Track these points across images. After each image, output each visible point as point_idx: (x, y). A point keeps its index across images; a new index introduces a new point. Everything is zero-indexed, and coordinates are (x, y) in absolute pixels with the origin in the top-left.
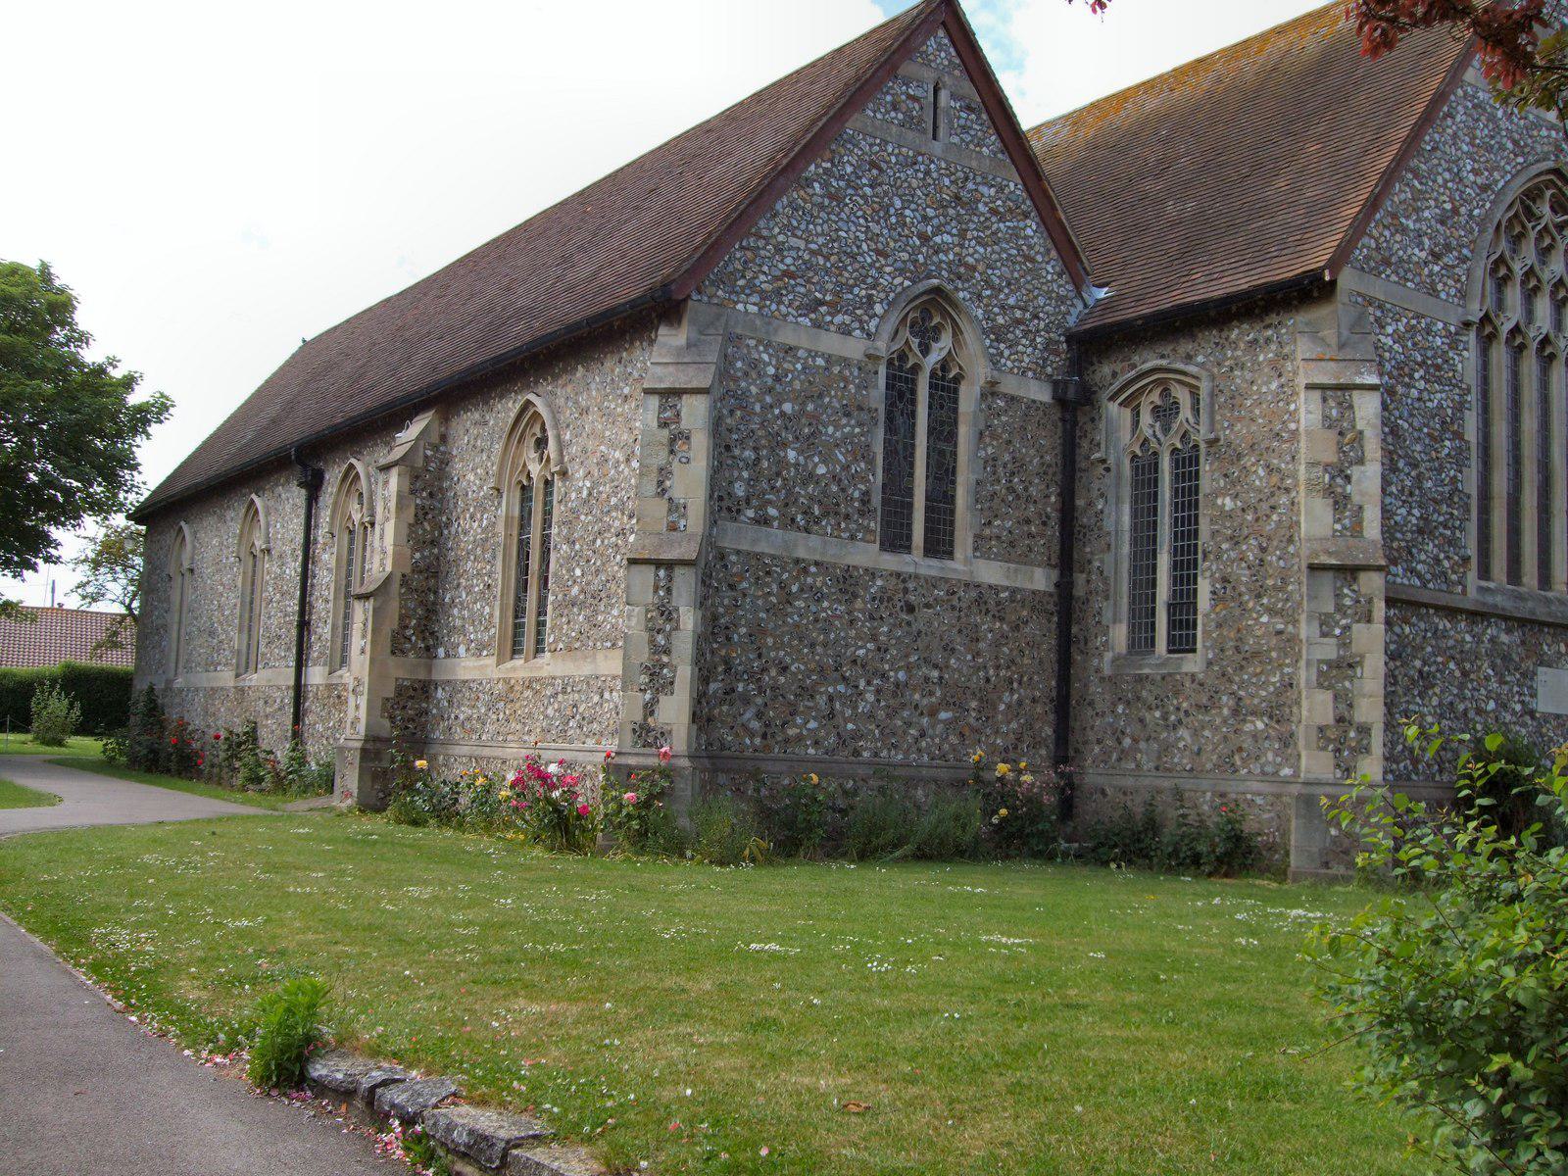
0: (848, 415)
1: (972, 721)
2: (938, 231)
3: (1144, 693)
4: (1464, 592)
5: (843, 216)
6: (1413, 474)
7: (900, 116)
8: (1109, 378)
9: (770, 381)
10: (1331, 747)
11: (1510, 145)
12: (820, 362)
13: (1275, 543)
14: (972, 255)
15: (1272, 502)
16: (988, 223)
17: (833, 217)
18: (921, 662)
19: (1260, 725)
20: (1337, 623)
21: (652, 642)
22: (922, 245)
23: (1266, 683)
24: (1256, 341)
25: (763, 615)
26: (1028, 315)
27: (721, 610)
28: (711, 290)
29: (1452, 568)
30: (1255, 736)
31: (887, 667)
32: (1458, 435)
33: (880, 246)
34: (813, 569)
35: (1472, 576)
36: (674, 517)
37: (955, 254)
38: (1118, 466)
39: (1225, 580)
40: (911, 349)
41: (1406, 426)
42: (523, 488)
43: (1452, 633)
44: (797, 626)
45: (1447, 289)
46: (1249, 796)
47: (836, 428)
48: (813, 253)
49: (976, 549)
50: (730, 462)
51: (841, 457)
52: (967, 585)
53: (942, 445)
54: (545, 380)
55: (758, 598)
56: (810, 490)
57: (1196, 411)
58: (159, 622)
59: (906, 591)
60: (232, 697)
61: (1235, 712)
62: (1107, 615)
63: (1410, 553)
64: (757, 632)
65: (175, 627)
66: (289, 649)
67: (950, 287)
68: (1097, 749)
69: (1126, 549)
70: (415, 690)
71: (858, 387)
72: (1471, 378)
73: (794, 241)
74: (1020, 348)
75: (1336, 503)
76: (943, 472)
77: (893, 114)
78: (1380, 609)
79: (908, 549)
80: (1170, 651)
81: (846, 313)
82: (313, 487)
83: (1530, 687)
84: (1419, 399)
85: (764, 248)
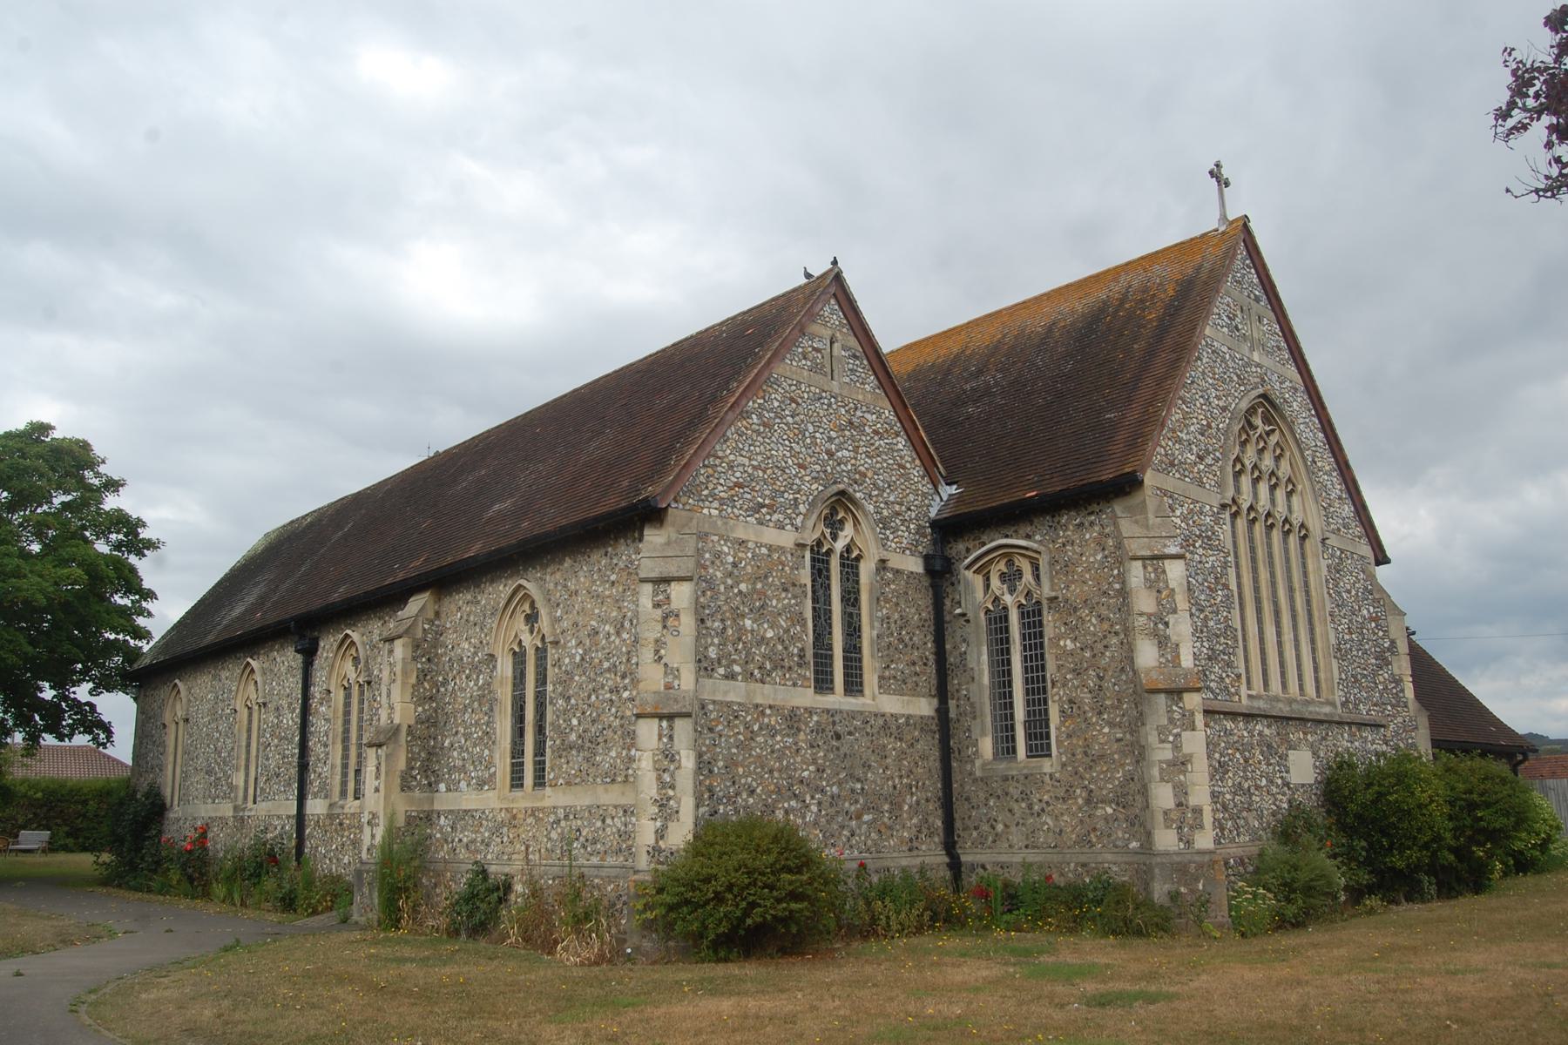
0: (786, 590)
1: (886, 820)
3: (1011, 790)
5: (773, 439)
6: (1202, 616)
7: (809, 363)
8: (964, 552)
9: (730, 567)
10: (1174, 826)
11: (1235, 378)
12: (764, 550)
14: (863, 465)
15: (1105, 642)
16: (872, 441)
17: (767, 440)
19: (1110, 811)
20: (1170, 732)
21: (659, 778)
22: (829, 459)
23: (1112, 778)
24: (1081, 524)
25: (734, 750)
26: (903, 508)
27: (704, 749)
28: (684, 499)
29: (1231, 684)
30: (1106, 818)
31: (824, 783)
32: (1226, 586)
33: (801, 461)
34: (768, 711)
35: (1244, 688)
37: (852, 465)
39: (1071, 702)
40: (825, 537)
41: (1194, 582)
42: (515, 653)
44: (759, 756)
45: (1209, 481)
46: (1106, 865)
48: (754, 468)
49: (880, 687)
51: (783, 623)
52: (876, 715)
53: (850, 609)
54: (534, 568)
55: (730, 737)
56: (763, 650)
57: (1037, 577)
58: (155, 762)
59: (834, 723)
60: (230, 824)
61: (1088, 801)
63: (1205, 675)
64: (731, 764)
65: (170, 767)
66: (289, 785)
67: (851, 490)
69: (986, 680)
70: (421, 819)
71: (792, 569)
72: (1229, 545)
75: (1160, 642)
76: (853, 630)
77: (804, 362)
78: (1199, 719)
79: (831, 690)
81: (780, 513)
84: (1200, 562)
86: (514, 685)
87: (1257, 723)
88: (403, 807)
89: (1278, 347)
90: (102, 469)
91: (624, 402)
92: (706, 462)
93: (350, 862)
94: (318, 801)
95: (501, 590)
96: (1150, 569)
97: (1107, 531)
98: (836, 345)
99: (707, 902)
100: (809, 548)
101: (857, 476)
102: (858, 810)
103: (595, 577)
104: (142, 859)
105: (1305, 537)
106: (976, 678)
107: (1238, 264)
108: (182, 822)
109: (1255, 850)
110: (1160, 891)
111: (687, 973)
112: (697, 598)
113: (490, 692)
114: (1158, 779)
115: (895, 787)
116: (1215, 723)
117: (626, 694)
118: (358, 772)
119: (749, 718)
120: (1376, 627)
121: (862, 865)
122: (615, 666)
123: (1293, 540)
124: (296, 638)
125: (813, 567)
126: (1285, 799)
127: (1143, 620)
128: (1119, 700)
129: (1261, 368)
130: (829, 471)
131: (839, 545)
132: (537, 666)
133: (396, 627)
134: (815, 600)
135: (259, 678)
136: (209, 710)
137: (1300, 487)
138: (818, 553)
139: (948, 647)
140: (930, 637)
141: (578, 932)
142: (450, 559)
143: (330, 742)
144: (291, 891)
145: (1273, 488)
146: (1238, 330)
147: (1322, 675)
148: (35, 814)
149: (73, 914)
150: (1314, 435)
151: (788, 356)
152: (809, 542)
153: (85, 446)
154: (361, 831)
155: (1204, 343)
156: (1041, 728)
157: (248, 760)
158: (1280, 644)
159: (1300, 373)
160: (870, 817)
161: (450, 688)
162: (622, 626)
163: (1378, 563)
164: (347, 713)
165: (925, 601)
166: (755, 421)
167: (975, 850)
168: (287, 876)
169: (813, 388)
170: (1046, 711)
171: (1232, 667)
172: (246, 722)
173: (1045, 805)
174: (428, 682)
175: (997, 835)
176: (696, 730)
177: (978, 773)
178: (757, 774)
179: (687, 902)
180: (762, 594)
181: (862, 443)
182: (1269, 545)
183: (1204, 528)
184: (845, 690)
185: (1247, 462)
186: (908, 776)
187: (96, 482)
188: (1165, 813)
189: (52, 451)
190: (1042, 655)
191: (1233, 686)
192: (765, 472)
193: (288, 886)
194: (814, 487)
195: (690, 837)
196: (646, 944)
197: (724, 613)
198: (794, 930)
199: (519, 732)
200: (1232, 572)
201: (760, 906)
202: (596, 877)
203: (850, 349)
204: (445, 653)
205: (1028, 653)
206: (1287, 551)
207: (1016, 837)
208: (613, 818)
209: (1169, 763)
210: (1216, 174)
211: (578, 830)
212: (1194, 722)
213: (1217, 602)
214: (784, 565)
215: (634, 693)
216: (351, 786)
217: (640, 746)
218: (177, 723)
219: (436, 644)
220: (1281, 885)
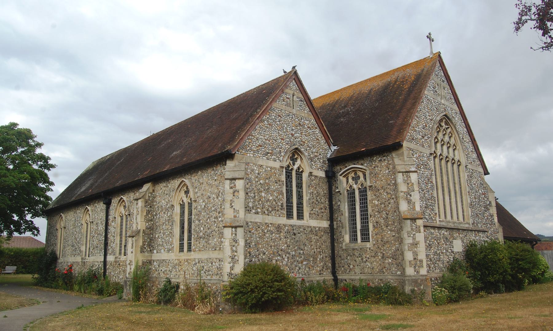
0: (276, 183)
1: (311, 264)
2: (296, 133)
4: (436, 222)
5: (272, 129)
6: (423, 193)
7: (285, 103)
8: (339, 170)
10: (413, 266)
11: (435, 109)
12: (269, 169)
15: (389, 202)
16: (307, 131)
17: (270, 130)
18: (298, 249)
19: (390, 261)
20: (412, 233)
21: (232, 249)
24: (381, 160)
25: (258, 239)
26: (318, 154)
27: (247, 238)
28: (241, 151)
31: (290, 251)
32: (432, 182)
33: (282, 137)
34: (270, 225)
36: (236, 213)
38: (343, 193)
39: (377, 222)
40: (290, 164)
42: (181, 205)
43: (435, 233)
44: (267, 241)
45: (426, 145)
46: (389, 280)
48: (266, 140)
49: (310, 217)
50: (248, 197)
51: (275, 194)
52: (308, 227)
53: (299, 190)
55: (257, 234)
56: (268, 204)
57: (365, 179)
59: (293, 230)
60: (80, 264)
61: (383, 257)
62: (343, 233)
63: (424, 213)
64: (257, 244)
65: (59, 244)
67: (300, 148)
68: (343, 269)
69: (347, 215)
70: (147, 263)
71: (279, 175)
72: (433, 168)
73: (261, 137)
74: (317, 163)
75: (408, 202)
76: (300, 197)
77: (283, 102)
78: (422, 229)
80: (362, 242)
81: (275, 155)
82: (108, 204)
83: (452, 245)
84: (423, 174)
85: (254, 139)
87: (442, 230)
88: (141, 258)
89: (450, 98)
90: (35, 139)
92: (249, 138)
93: (122, 278)
94: (111, 256)
95: (175, 183)
96: (405, 176)
97: (390, 162)
98: (295, 97)
99: (248, 292)
100: (285, 168)
101: (302, 143)
102: (301, 260)
103: (209, 178)
104: (49, 276)
106: (343, 214)
107: (437, 69)
108: (63, 263)
109: (441, 275)
110: (408, 289)
112: (245, 185)
113: (172, 218)
115: (315, 252)
116: (428, 230)
117: (220, 219)
118: (125, 246)
119: (263, 228)
120: (484, 197)
122: (216, 209)
123: (455, 166)
125: (286, 175)
126: (452, 257)
127: (402, 194)
129: (444, 105)
130: (292, 141)
131: (295, 167)
132: (189, 209)
134: (287, 186)
135: (90, 213)
137: (458, 148)
138: (288, 170)
139: (333, 203)
140: (327, 200)
141: (203, 302)
142: (158, 171)
143: (115, 235)
144: (102, 288)
146: (436, 92)
147: (465, 214)
149: (25, 296)
151: (278, 100)
152: (285, 166)
153: (29, 131)
154: (127, 267)
155: (424, 97)
157: (86, 242)
160: (306, 263)
162: (219, 195)
163: (485, 174)
164: (121, 225)
165: (325, 187)
166: (266, 123)
167: (343, 275)
168: (100, 282)
169: (286, 112)
171: (433, 211)
172: (86, 228)
173: (367, 259)
174: (150, 214)
175: (350, 269)
176: (245, 232)
177: (344, 248)
178: (266, 247)
179: (241, 292)
181: (304, 131)
182: (447, 168)
183: (424, 162)
184: (297, 218)
185: (439, 139)
186: (319, 248)
187: (33, 144)
188: (410, 262)
190: (367, 206)
191: (434, 217)
192: (269, 141)
194: (287, 146)
195: (242, 269)
199: (182, 232)
200: (434, 177)
201: (267, 294)
202: (209, 283)
203: (300, 98)
205: (362, 205)
206: (453, 170)
207: (357, 270)
208: (215, 263)
210: (429, 37)
211: (203, 267)
213: (429, 188)
214: (276, 174)
215: (223, 219)
216: (123, 251)
218: (61, 229)
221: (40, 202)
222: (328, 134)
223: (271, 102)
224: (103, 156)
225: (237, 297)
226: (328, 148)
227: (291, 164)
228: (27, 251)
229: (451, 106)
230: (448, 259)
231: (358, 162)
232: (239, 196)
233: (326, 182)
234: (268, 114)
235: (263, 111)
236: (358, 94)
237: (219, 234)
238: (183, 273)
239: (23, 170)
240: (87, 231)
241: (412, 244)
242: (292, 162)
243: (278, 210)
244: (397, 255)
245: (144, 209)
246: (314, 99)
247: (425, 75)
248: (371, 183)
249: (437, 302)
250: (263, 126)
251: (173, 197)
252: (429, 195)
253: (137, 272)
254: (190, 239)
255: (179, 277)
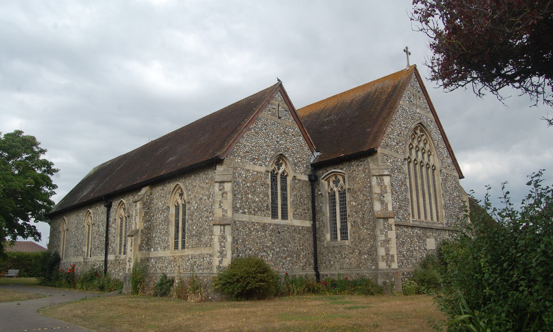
0: (262, 186)
1: (295, 260)
2: (281, 140)
4: (410, 222)
5: (259, 137)
6: (397, 195)
7: (271, 113)
8: (321, 174)
9: (244, 178)
11: (410, 118)
12: (255, 173)
13: (366, 213)
15: (365, 203)
19: (366, 257)
20: (384, 231)
21: (220, 244)
22: (277, 144)
24: (358, 165)
25: (245, 236)
26: (302, 160)
27: (235, 236)
28: (229, 156)
29: (406, 216)
31: (274, 248)
32: (405, 185)
34: (256, 224)
35: (411, 218)
36: (224, 213)
39: (354, 222)
40: (276, 169)
42: (176, 206)
44: (253, 238)
45: (400, 151)
46: (365, 274)
47: (260, 189)
48: (252, 146)
49: (293, 217)
51: (261, 196)
52: (292, 226)
53: (284, 192)
55: (244, 232)
57: (344, 182)
59: (278, 228)
60: (82, 264)
61: (359, 254)
62: (325, 232)
63: (398, 213)
64: (244, 241)
65: (62, 246)
66: (102, 250)
67: (284, 154)
68: (324, 265)
69: (328, 215)
70: (145, 260)
71: (264, 179)
72: (407, 172)
74: (300, 168)
75: (381, 202)
76: (284, 199)
77: (269, 112)
79: (277, 218)
82: (109, 207)
84: (397, 177)
86: (176, 216)
87: (416, 229)
88: (140, 256)
89: (426, 107)
90: (39, 146)
91: (212, 125)
92: (237, 145)
93: (122, 275)
94: (112, 255)
95: (171, 186)
96: (379, 179)
97: (366, 167)
98: (280, 107)
99: (234, 282)
100: (270, 172)
101: (286, 149)
102: (285, 256)
103: (201, 181)
104: (53, 276)
105: (434, 169)
106: (325, 214)
107: (412, 80)
108: (66, 264)
109: (413, 270)
110: (380, 282)
111: (226, 304)
112: (233, 188)
113: (168, 219)
114: (380, 246)
115: (298, 249)
116: (401, 229)
117: (211, 219)
118: (125, 246)
119: (250, 226)
120: (459, 199)
121: (286, 274)
122: (207, 209)
123: (430, 171)
124: (105, 202)
125: (271, 178)
126: (425, 254)
127: (376, 195)
128: (369, 221)
129: (420, 114)
130: (277, 147)
131: (280, 171)
132: (183, 210)
133: (138, 198)
134: (272, 189)
135: (92, 216)
136: (75, 227)
137: (433, 153)
138: (273, 174)
139: (316, 204)
140: (310, 201)
141: (194, 293)
142: (155, 176)
143: (116, 236)
144: (103, 284)
145: (423, 154)
146: (412, 102)
147: (439, 215)
148: (14, 264)
149: (32, 292)
150: (438, 136)
151: (264, 110)
152: (270, 170)
153: (34, 138)
154: (126, 265)
155: (399, 106)
156: (345, 230)
157: (88, 243)
158: (424, 204)
159: (434, 116)
160: (290, 259)
161: (155, 218)
162: (210, 197)
163: (460, 178)
164: (121, 226)
165: (309, 190)
166: (253, 131)
167: (324, 270)
168: (101, 279)
169: (272, 121)
170: (347, 225)
171: (407, 211)
172: (87, 230)
173: (346, 255)
174: (148, 215)
175: (331, 265)
176: (232, 230)
177: (326, 245)
178: (252, 244)
179: (229, 283)
180: (255, 187)
181: (288, 139)
182: (421, 172)
183: (398, 166)
184: (282, 218)
185: (414, 145)
186: (302, 246)
187: (37, 150)
188: (382, 257)
189: (23, 140)
190: (346, 207)
191: (407, 217)
192: (256, 148)
193: (102, 283)
194: (272, 153)
195: (230, 263)
196: (216, 296)
197: (242, 192)
198: (262, 291)
199: (177, 231)
200: (408, 180)
201: (251, 283)
202: (201, 277)
203: (285, 108)
204: (154, 206)
205: (341, 206)
206: (427, 174)
207: (337, 266)
208: (206, 258)
209: (384, 241)
210: (406, 51)
211: (196, 262)
212: (392, 228)
213: (402, 190)
214: (262, 178)
215: (213, 218)
216: (123, 250)
217: (214, 234)
218: (64, 231)
219: (151, 203)
220: (421, 280)
221: (41, 207)
222: (311, 141)
223: (258, 112)
224: (103, 163)
225: (224, 287)
226: (311, 154)
227: (277, 168)
228: (29, 255)
229: (426, 115)
230: (421, 255)
231: (338, 167)
232: (227, 197)
233: (309, 186)
234: (255, 123)
235: (250, 120)
236: (341, 104)
237: (209, 232)
238: (178, 268)
239: (28, 176)
240: (89, 233)
241: (384, 241)
242: (277, 167)
243: (263, 211)
244: (372, 251)
245: (142, 211)
246: (298, 110)
247: (401, 87)
248: (349, 186)
249: (406, 293)
250: (250, 134)
251: (169, 199)
252: (403, 196)
253: (136, 268)
254: (184, 237)
255: (174, 272)
